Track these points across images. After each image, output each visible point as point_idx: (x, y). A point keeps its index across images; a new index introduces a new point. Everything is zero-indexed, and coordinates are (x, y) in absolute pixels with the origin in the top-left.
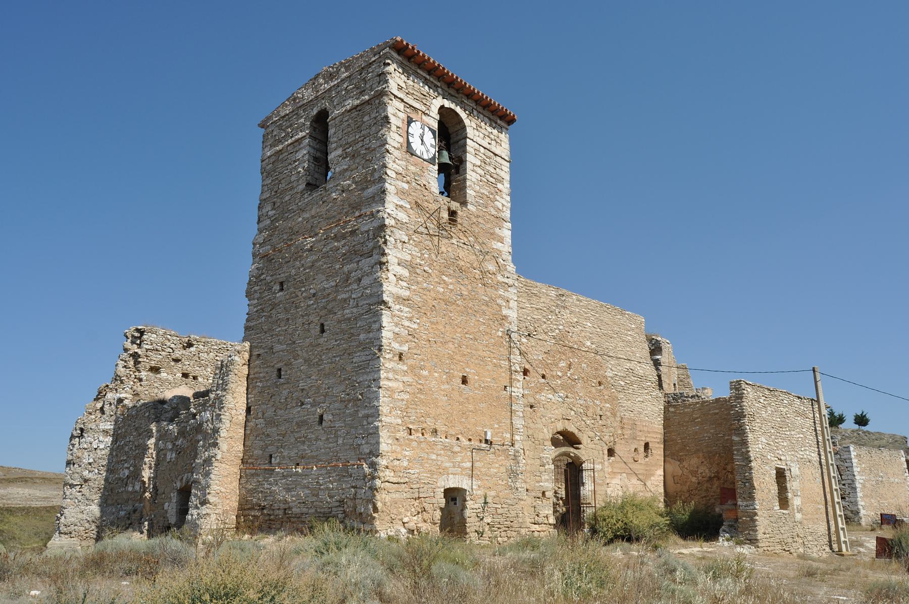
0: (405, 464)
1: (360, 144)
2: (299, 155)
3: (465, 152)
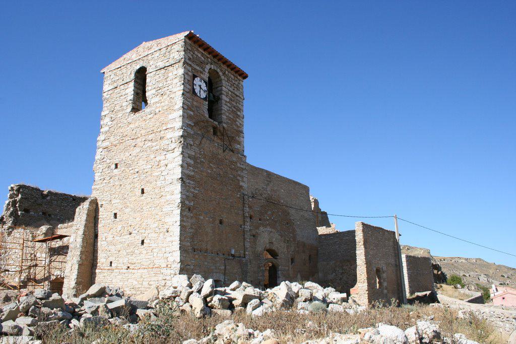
0: (192, 267)
1: (166, 88)
2: (127, 91)
3: (221, 94)
